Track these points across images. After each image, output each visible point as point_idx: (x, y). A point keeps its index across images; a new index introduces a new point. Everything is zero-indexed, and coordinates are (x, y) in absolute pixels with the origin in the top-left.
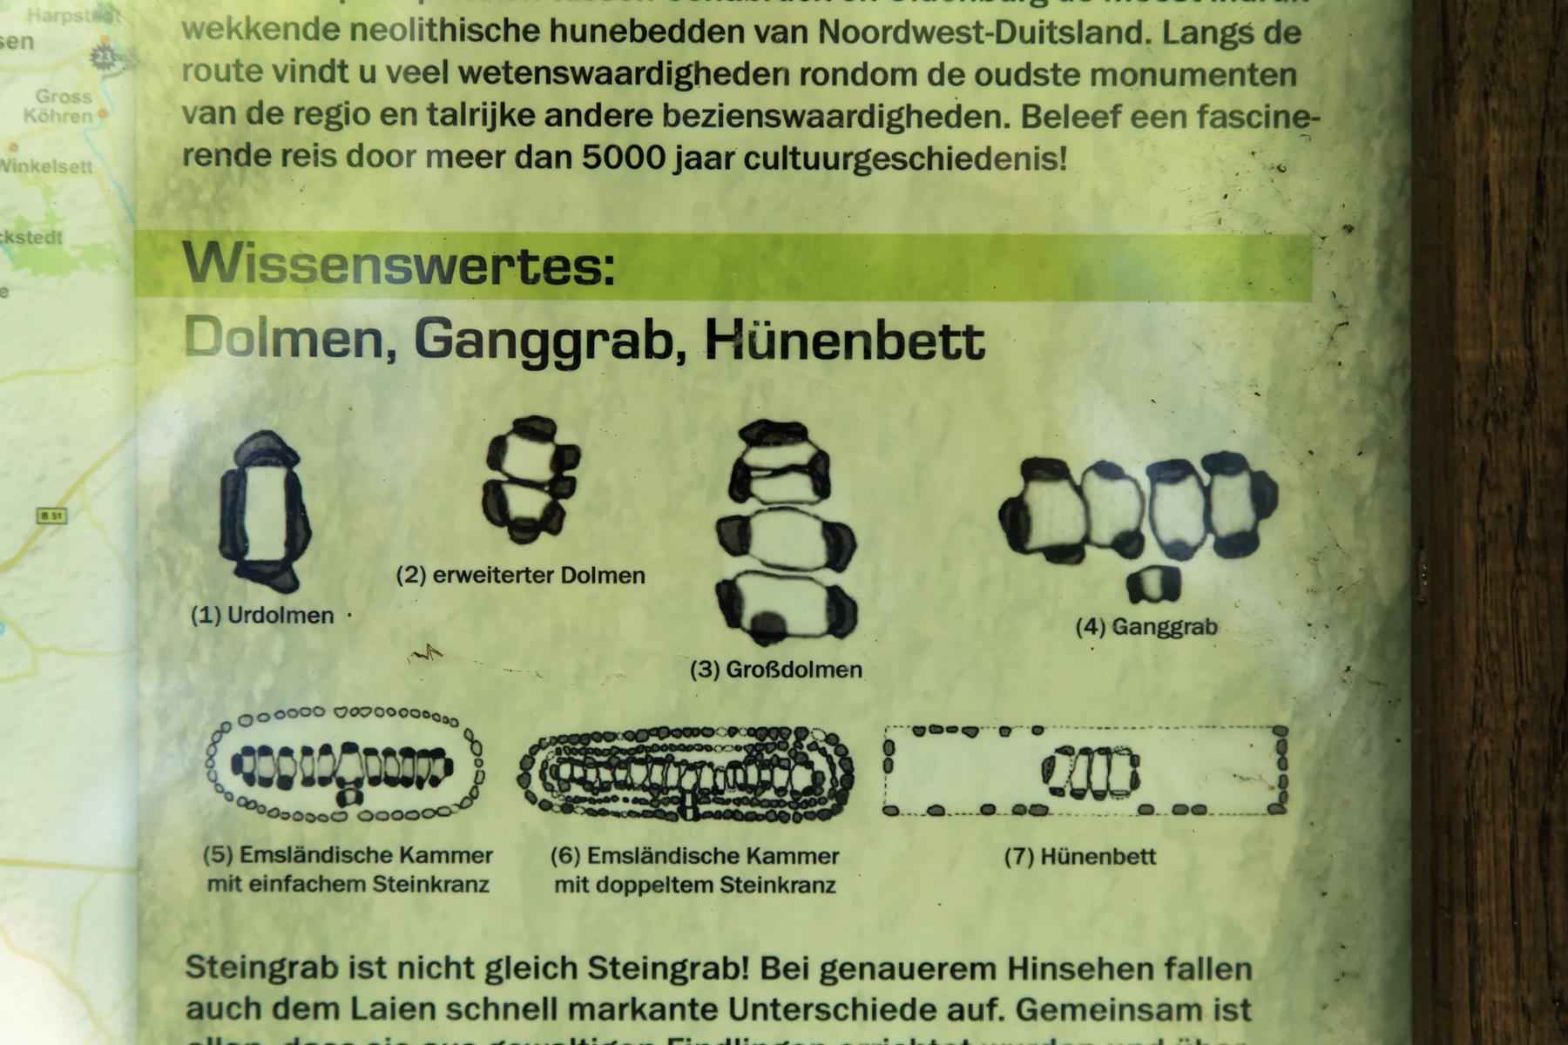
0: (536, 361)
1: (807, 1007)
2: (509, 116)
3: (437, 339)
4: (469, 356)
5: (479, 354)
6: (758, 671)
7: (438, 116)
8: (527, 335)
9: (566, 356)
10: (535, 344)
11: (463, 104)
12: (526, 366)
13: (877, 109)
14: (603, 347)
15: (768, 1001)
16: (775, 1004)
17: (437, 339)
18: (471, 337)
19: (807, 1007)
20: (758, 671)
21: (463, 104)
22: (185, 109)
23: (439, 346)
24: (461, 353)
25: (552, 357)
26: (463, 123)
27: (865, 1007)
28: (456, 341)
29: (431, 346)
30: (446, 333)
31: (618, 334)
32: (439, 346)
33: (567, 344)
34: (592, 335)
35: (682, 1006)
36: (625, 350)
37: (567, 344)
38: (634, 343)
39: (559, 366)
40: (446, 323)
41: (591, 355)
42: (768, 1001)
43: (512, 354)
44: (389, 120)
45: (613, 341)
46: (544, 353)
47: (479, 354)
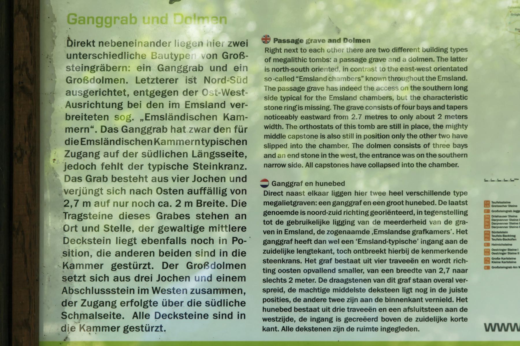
0: (100, 25)
1: (90, 55)
2: (176, 316)
3: (73, 19)
4: (81, 24)
5: (84, 23)
6: (236, 56)
7: (449, 107)
8: (97, 18)
9: (108, 23)
10: (99, 20)
11: (93, 288)
12: (97, 26)
13: (193, 301)
14: (118, 21)
15: (78, 53)
16: (80, 54)
17: (73, 19)
18: (82, 19)
19: (90, 55)
20: (236, 56)
21: (93, 288)
22: (231, 190)
23: (74, 21)
24: (79, 23)
25: (104, 24)
26: (224, 306)
27: (107, 55)
28: (78, 20)
29: (71, 21)
30: (75, 18)
31: (122, 18)
32: (74, 21)
33: (108, 20)
34: (115, 18)
35: (76, 54)
36: (124, 22)
37: (108, 20)
38: (127, 20)
39: (106, 26)
40: (75, 15)
41: (115, 23)
42: (78, 53)
43: (93, 23)
44: (219, 280)
45: (121, 19)
46: (102, 23)
47: (84, 23)
